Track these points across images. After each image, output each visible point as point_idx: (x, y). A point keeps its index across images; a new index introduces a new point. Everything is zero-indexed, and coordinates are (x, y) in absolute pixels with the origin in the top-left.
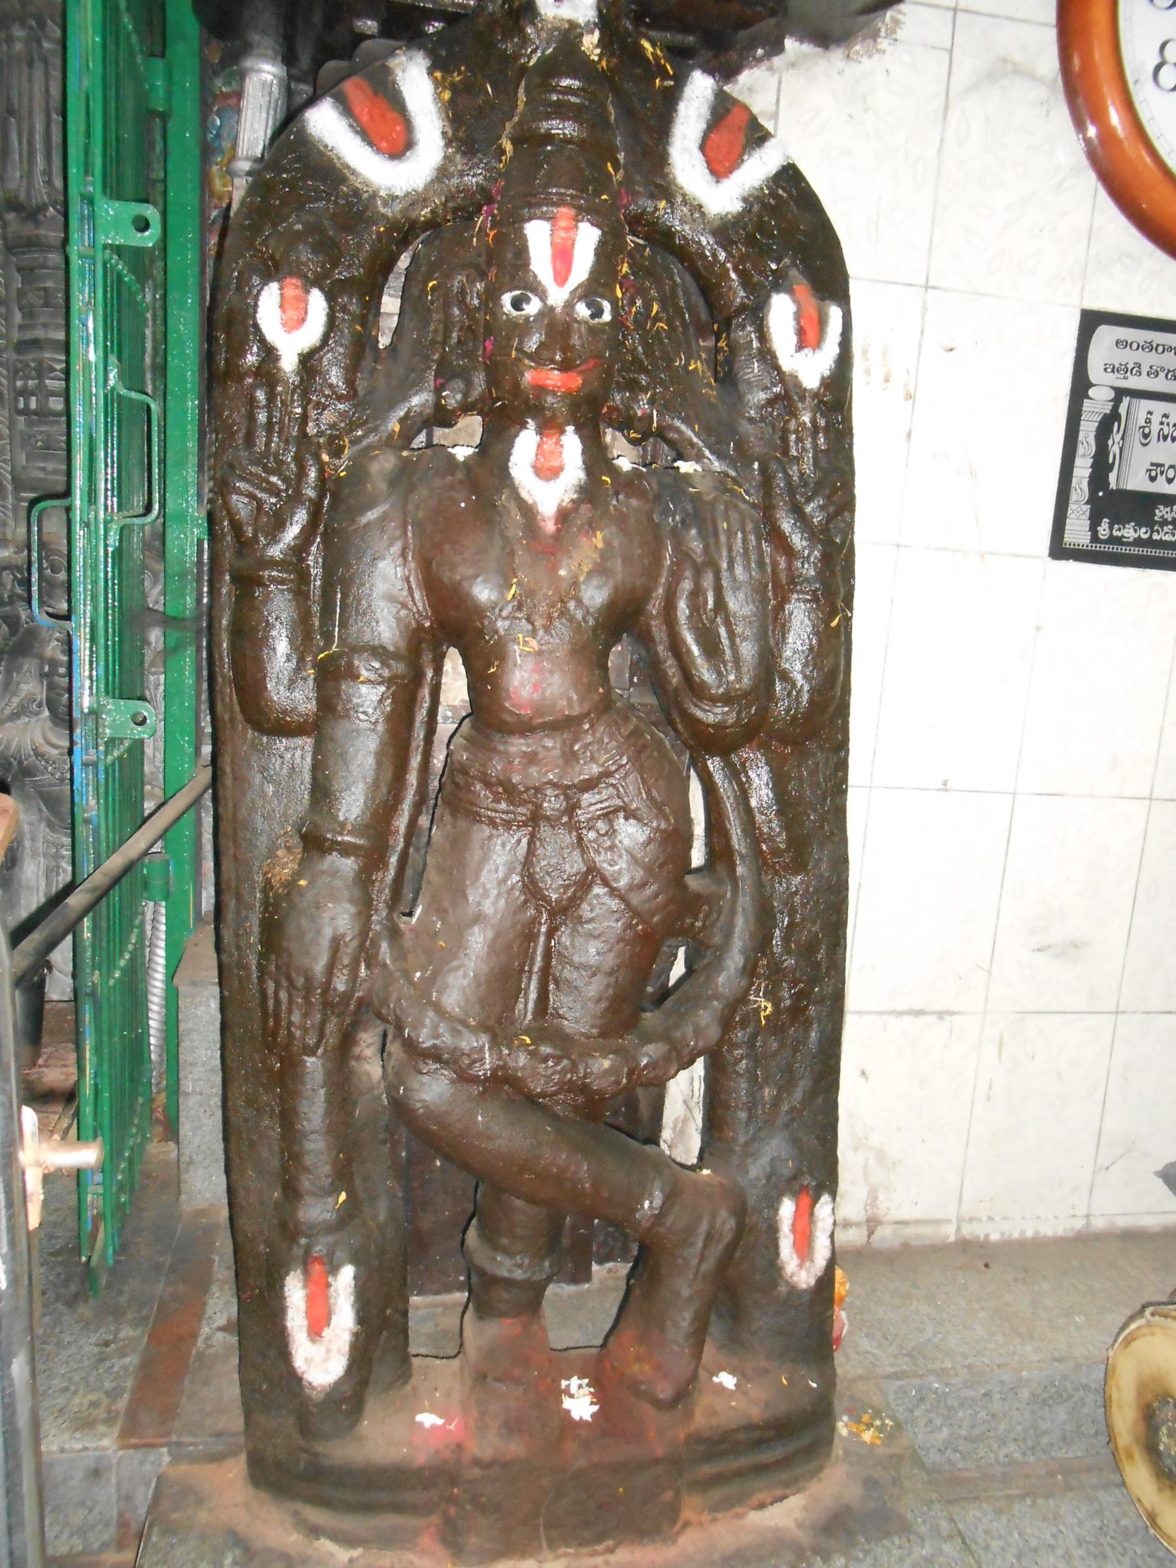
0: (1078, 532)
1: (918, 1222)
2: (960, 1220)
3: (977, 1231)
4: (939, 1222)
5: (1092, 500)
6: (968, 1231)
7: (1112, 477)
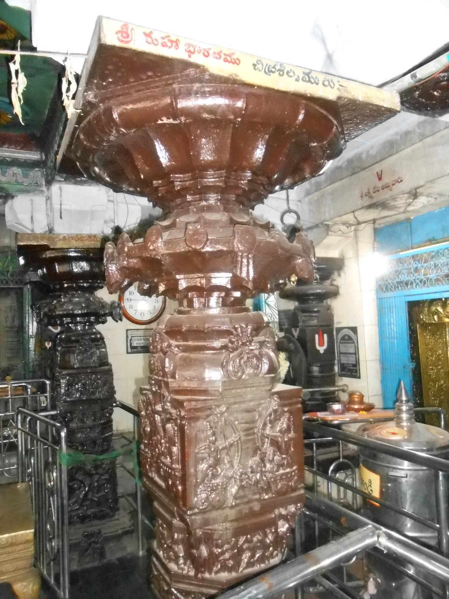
0: (129, 350)
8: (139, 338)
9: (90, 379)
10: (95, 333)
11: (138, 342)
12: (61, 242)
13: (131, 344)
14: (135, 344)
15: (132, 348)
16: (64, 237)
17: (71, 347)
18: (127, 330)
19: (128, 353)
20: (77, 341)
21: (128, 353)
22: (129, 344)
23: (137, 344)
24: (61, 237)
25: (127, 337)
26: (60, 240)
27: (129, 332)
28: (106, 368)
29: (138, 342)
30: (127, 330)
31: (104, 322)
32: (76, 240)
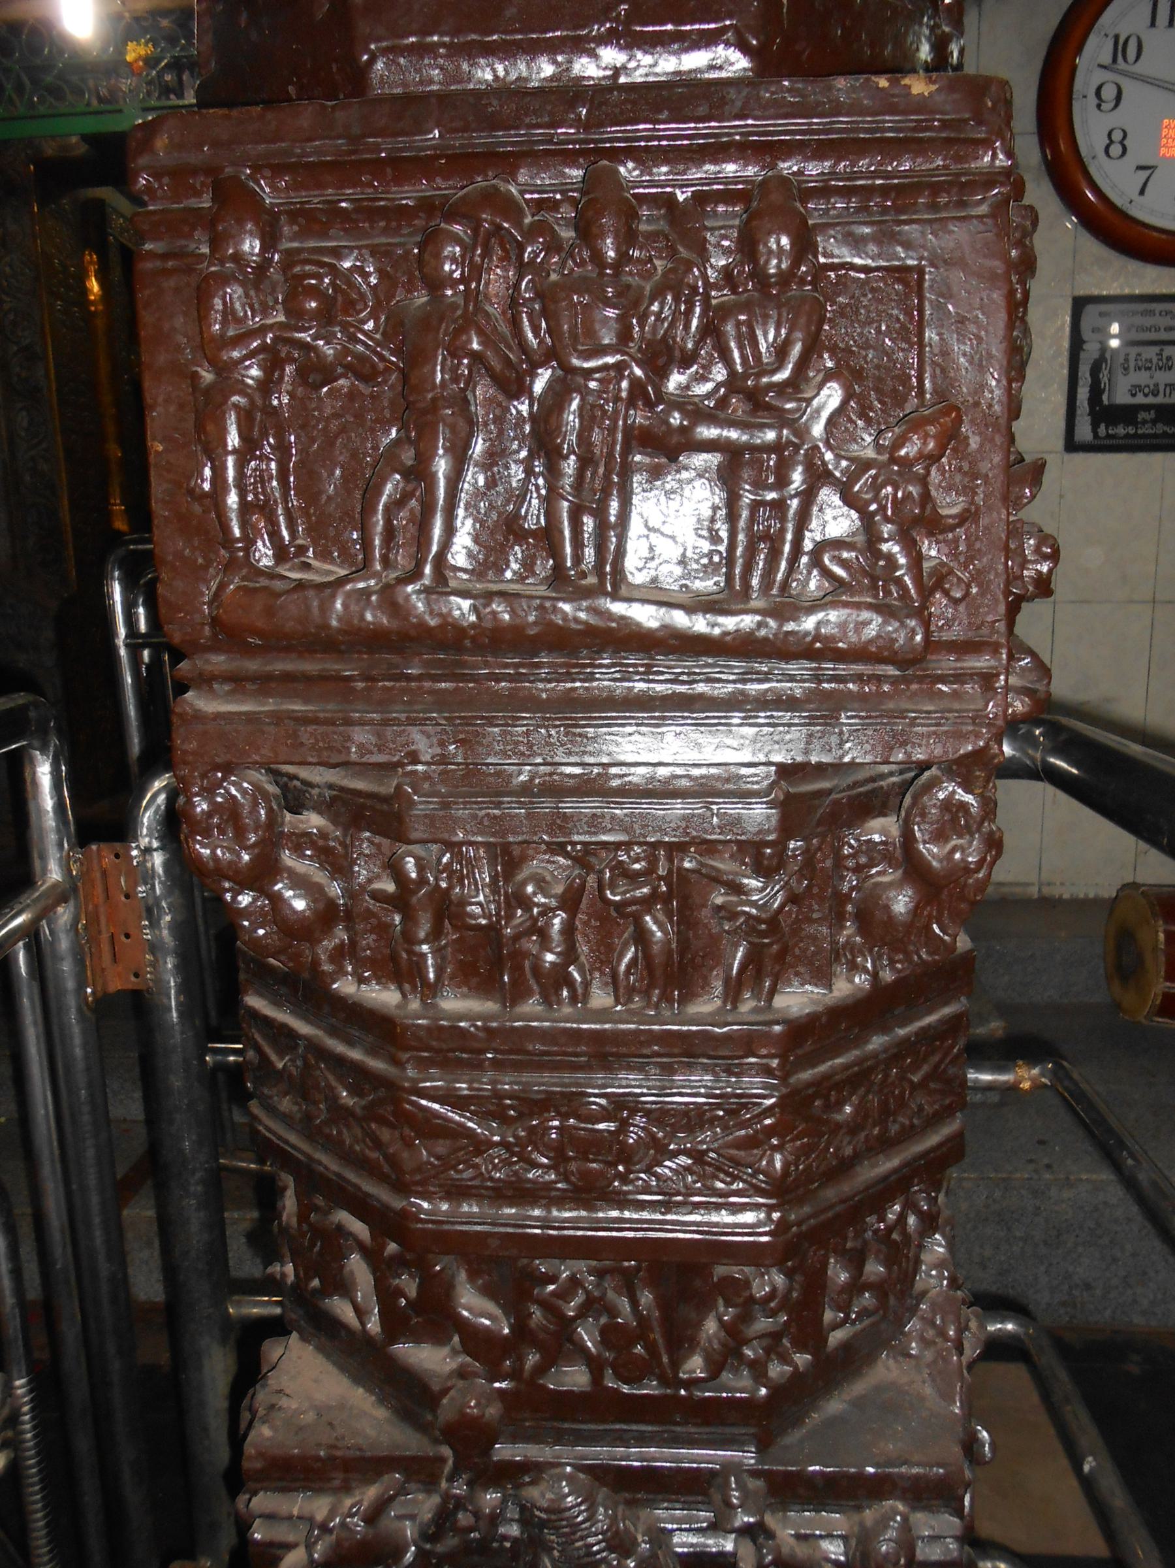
0: (1084, 431)
1: (1011, 884)
2: (1041, 885)
3: (1055, 892)
4: (1027, 885)
5: (1092, 413)
6: (1046, 891)
7: (1105, 397)
11: (1142, 378)
15: (1103, 413)
22: (1083, 393)
23: (1135, 390)
29: (1142, 378)
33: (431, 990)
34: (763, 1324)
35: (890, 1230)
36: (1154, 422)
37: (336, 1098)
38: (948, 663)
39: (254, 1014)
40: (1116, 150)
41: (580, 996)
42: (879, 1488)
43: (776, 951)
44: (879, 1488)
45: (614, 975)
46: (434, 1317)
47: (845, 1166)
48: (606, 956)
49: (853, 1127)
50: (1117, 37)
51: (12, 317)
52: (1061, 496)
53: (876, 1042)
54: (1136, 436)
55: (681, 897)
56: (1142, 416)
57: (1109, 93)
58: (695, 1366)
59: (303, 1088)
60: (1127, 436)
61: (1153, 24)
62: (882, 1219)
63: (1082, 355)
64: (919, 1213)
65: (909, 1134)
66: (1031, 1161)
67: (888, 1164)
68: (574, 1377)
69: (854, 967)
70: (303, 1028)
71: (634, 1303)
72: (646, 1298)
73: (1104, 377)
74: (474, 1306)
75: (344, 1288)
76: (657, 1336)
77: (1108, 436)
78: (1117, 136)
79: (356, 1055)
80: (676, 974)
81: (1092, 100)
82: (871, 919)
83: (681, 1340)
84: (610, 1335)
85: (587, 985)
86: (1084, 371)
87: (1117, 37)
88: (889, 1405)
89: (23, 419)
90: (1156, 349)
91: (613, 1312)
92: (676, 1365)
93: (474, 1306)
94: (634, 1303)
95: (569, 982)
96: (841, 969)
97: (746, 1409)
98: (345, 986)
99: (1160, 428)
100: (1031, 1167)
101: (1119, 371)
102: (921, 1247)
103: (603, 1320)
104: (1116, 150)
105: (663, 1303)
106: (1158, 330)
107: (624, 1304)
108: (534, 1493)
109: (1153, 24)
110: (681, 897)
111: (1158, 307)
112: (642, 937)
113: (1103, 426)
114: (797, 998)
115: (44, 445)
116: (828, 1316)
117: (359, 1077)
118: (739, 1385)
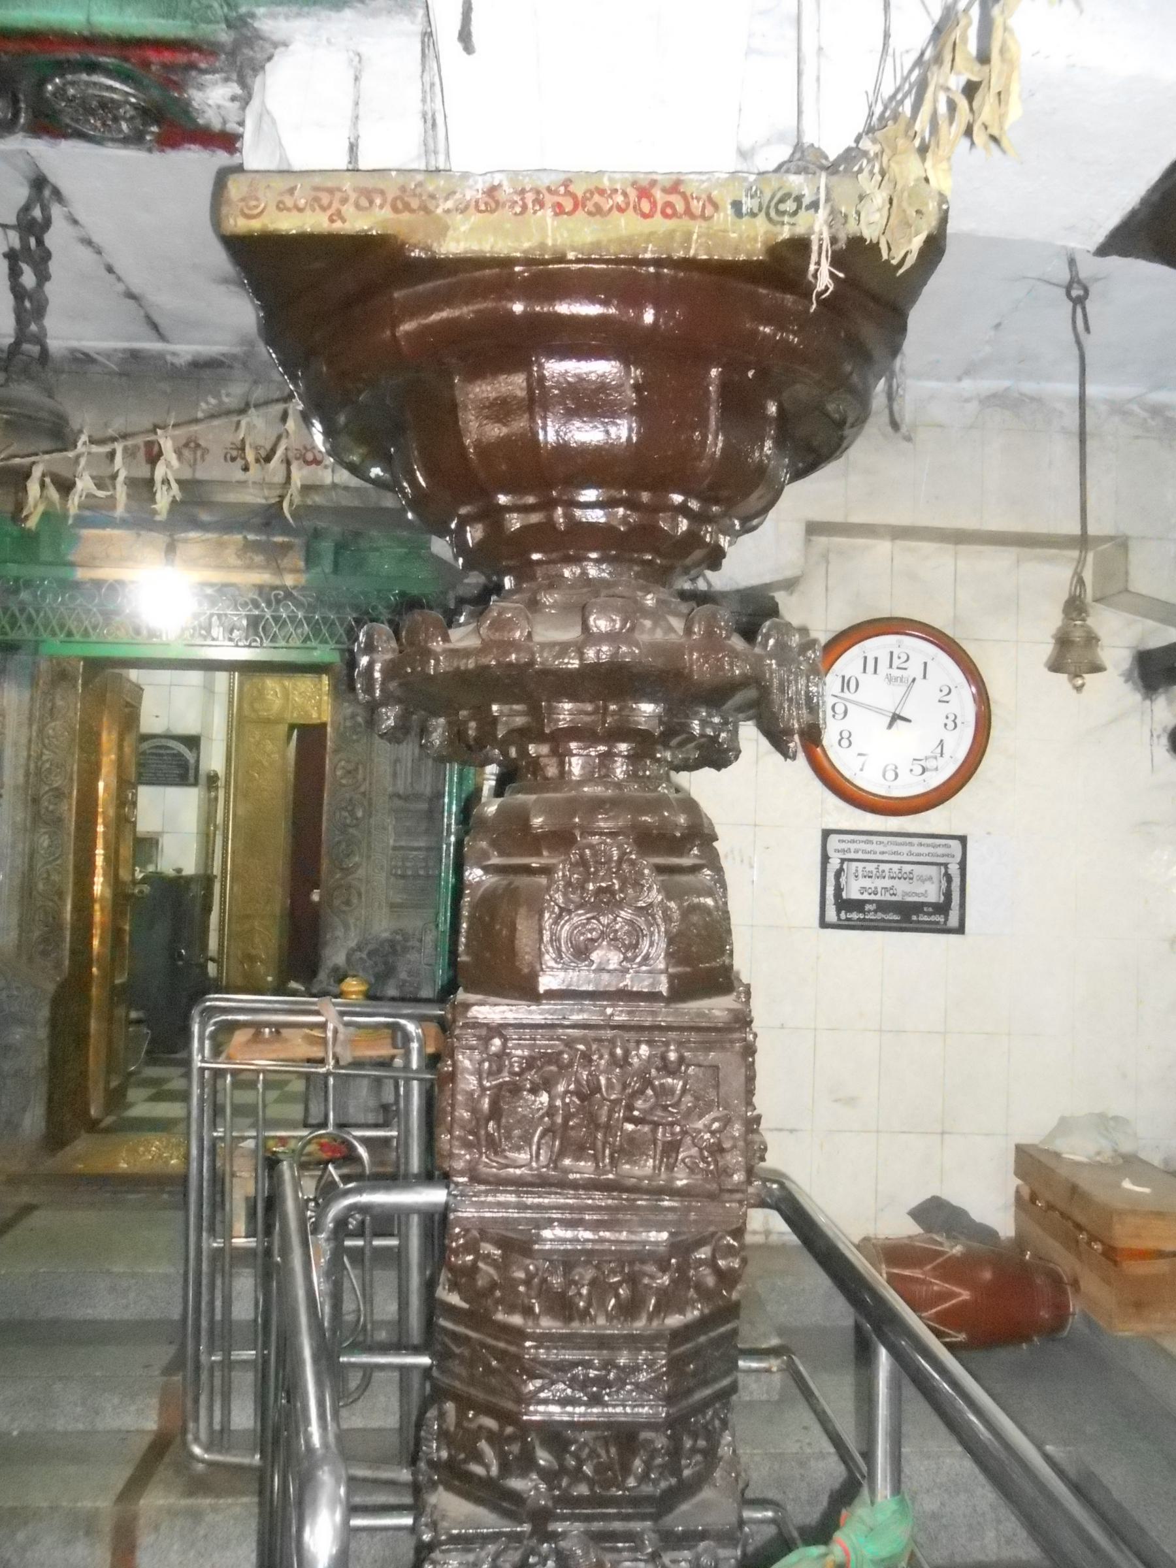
0: (831, 915)
8: (871, 867)
9: (625, 1062)
10: (660, 803)
11: (867, 883)
12: (475, 218)
13: (838, 889)
14: (853, 892)
15: (843, 904)
16: (492, 191)
17: (527, 870)
18: (826, 834)
19: (824, 924)
20: (561, 839)
21: (824, 924)
22: (830, 891)
23: (863, 890)
24: (473, 191)
25: (825, 858)
26: (463, 210)
27: (833, 840)
28: (718, 1007)
29: (867, 883)
30: (826, 834)
31: (717, 756)
32: (559, 210)
33: (536, 1318)
34: (659, 1461)
35: (707, 1423)
36: (875, 911)
37: (490, 1364)
38: (726, 1196)
39: (445, 1330)
40: (845, 743)
41: (593, 1320)
42: (703, 1536)
43: (668, 1301)
44: (703, 1536)
45: (607, 1311)
46: (527, 1463)
47: (689, 1392)
48: (603, 1304)
49: (694, 1374)
50: (843, 677)
51: (47, 765)
52: (818, 958)
53: (702, 1339)
54: (864, 920)
55: (632, 1280)
56: (868, 907)
57: (840, 709)
58: (631, 1482)
59: (471, 1364)
60: (859, 920)
61: (865, 671)
62: (704, 1418)
63: (829, 866)
64: (720, 1419)
65: (715, 1379)
66: (798, 1441)
67: (707, 1392)
68: (583, 1490)
69: (694, 1308)
70: (473, 1334)
71: (608, 1452)
72: (613, 1450)
73: (843, 880)
74: (544, 1458)
75: (478, 1458)
76: (617, 1467)
77: (848, 919)
78: (845, 735)
79: (502, 1345)
80: (629, 1309)
81: (829, 713)
82: (699, 1287)
83: (626, 1470)
84: (598, 1469)
85: (596, 1315)
86: (831, 876)
87: (843, 677)
88: (705, 1506)
89: (45, 841)
90: (876, 865)
91: (599, 1456)
92: (624, 1480)
93: (544, 1458)
94: (608, 1452)
95: (589, 1314)
96: (689, 1309)
97: (649, 1499)
98: (500, 1316)
99: (880, 916)
100: (799, 1445)
101: (852, 878)
102: (721, 1435)
103: (595, 1461)
104: (845, 743)
105: (620, 1454)
106: (875, 853)
107: (603, 1453)
108: (562, 1544)
109: (865, 671)
110: (632, 1280)
111: (874, 838)
112: (617, 1296)
113: (843, 913)
114: (674, 1320)
115: (58, 862)
116: (684, 1462)
117: (502, 1355)
118: (648, 1489)
